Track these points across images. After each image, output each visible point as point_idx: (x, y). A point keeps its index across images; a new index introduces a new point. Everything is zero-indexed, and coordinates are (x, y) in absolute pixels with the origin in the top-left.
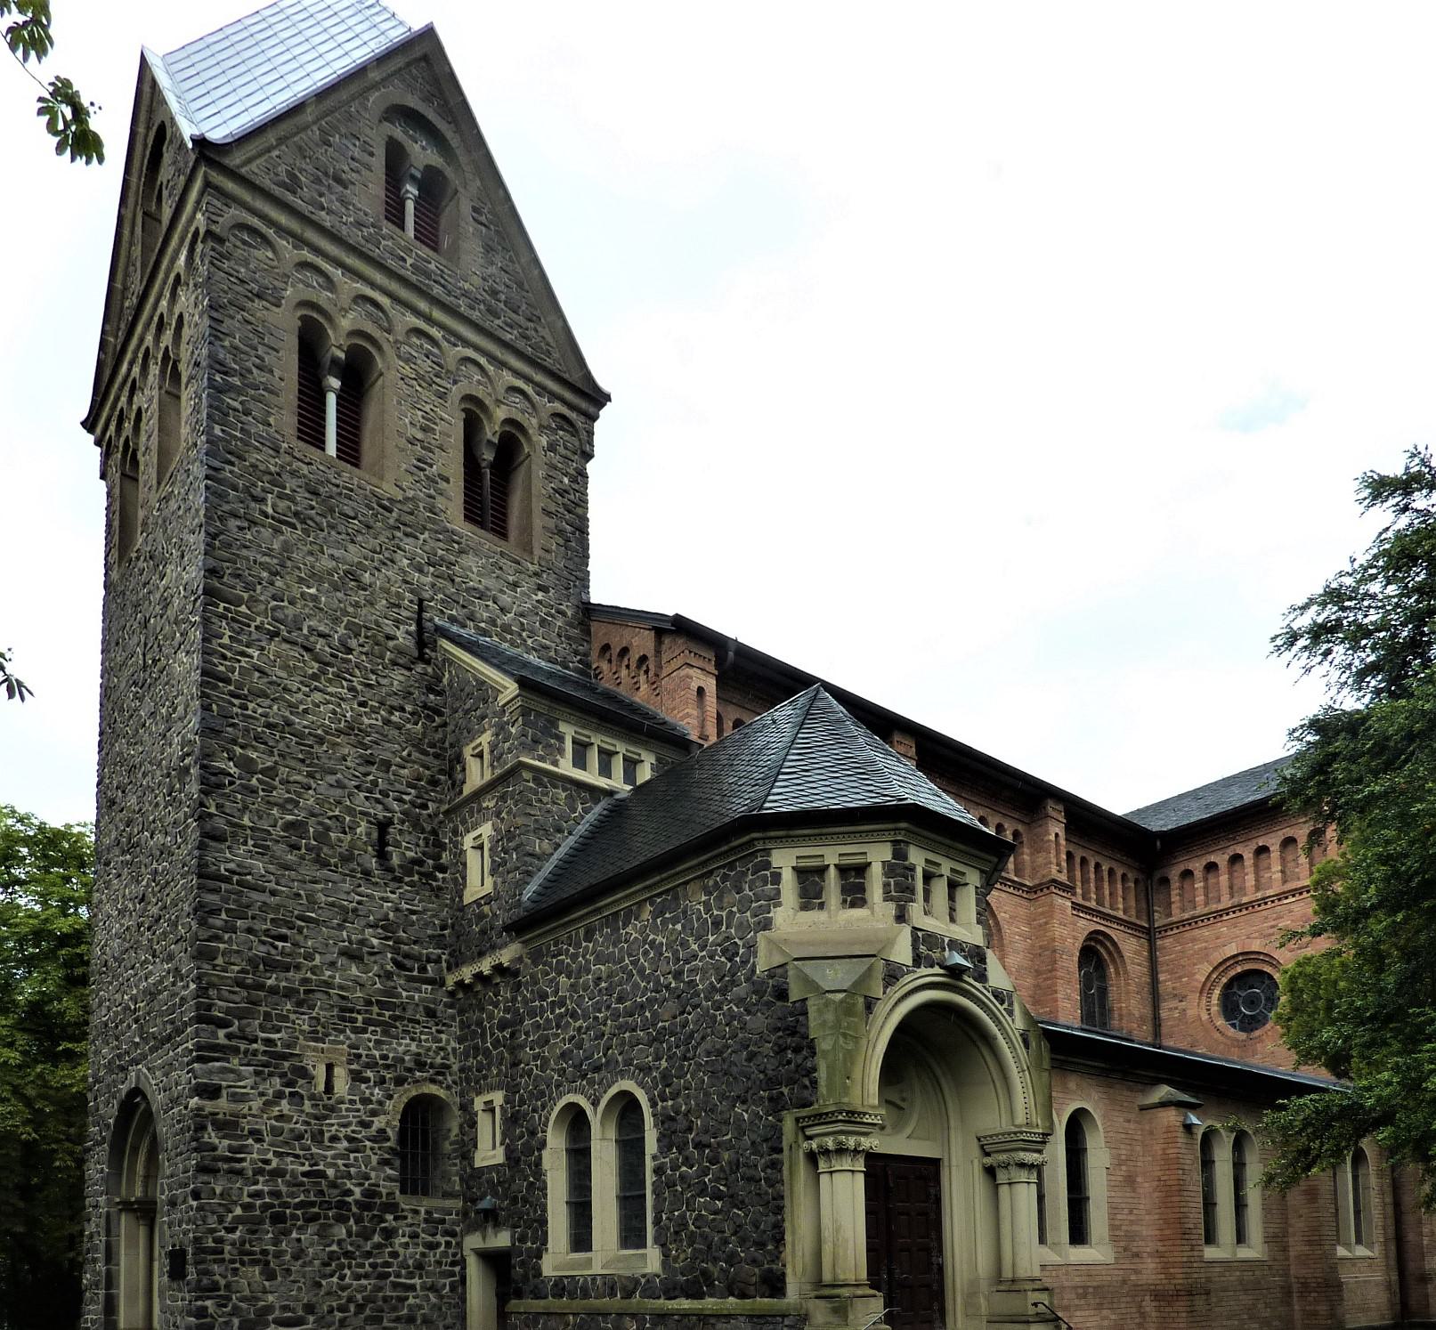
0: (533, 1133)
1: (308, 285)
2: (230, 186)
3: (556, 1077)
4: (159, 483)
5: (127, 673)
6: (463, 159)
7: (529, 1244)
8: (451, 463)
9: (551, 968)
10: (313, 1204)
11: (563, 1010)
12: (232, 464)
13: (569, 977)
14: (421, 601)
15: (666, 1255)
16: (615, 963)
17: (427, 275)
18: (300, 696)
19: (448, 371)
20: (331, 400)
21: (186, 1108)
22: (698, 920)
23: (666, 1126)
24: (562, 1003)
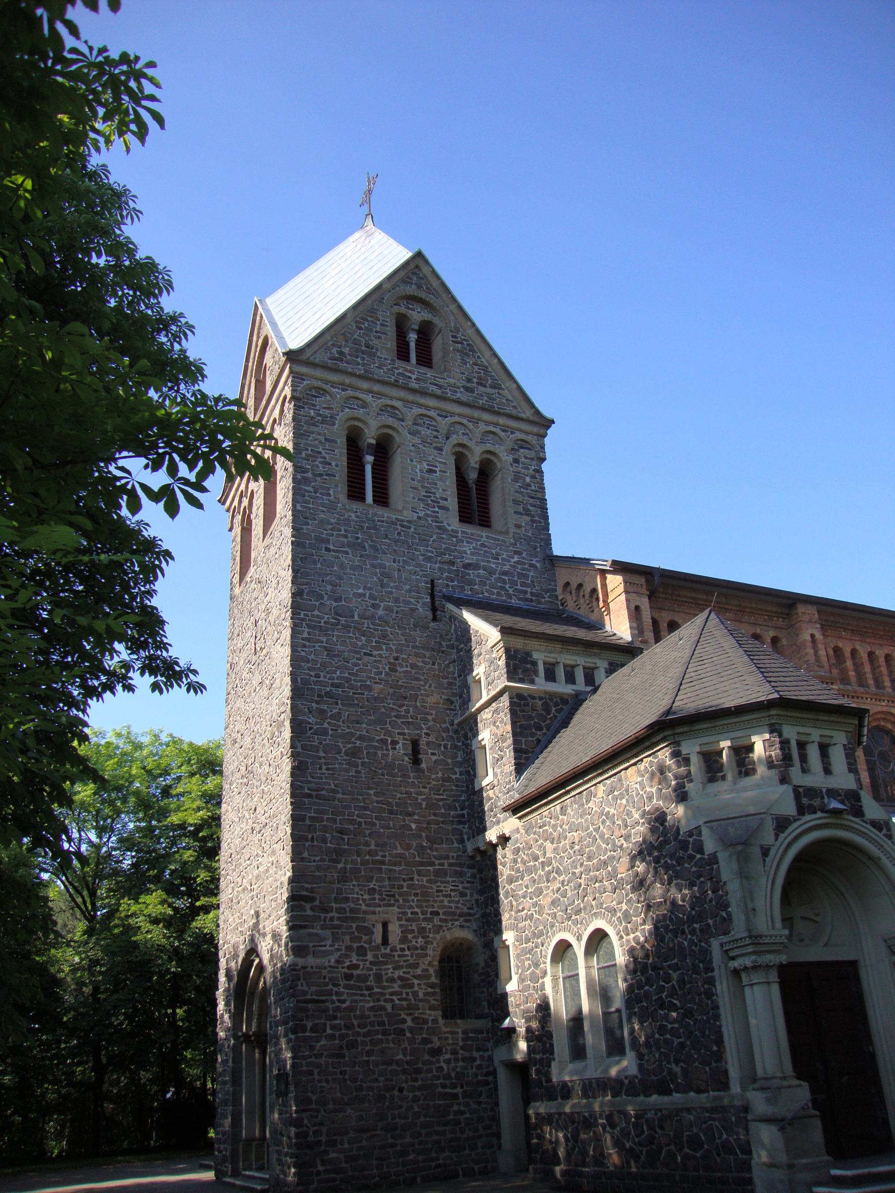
4: (264, 537)
5: (244, 655)
8: (447, 489)
10: (377, 1032)
13: (552, 843)
14: (432, 582)
15: (640, 1057)
20: (368, 469)
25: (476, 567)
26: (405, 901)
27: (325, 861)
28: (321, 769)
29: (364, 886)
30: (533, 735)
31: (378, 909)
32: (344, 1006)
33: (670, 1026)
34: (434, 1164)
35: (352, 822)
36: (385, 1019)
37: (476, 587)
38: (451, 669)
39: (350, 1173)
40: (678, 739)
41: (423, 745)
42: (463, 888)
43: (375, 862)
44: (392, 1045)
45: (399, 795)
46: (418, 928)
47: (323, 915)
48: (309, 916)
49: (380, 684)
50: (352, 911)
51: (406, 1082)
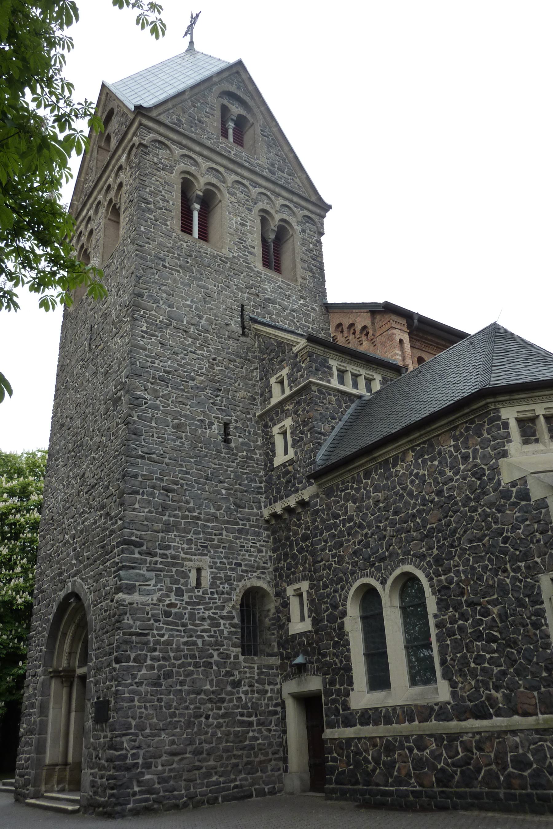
0: (335, 607)
1: (186, 164)
2: (151, 124)
3: (350, 567)
6: (256, 110)
7: (338, 686)
9: (341, 498)
10: (189, 664)
11: (352, 524)
12: (149, 244)
13: (355, 502)
14: (243, 306)
15: (453, 685)
16: (389, 490)
17: (241, 158)
18: (182, 355)
19: (252, 199)
20: (196, 215)
21: (112, 601)
22: (450, 457)
23: (442, 593)
24: (351, 519)
25: (273, 302)
26: (216, 552)
27: (152, 513)
28: (152, 436)
29: (183, 537)
30: (329, 422)
31: (193, 557)
32: (163, 639)
33: (488, 656)
34: (232, 785)
35: (176, 483)
36: (197, 653)
37: (274, 316)
38: (255, 374)
39: (162, 794)
40: (498, 406)
41: (232, 429)
42: (260, 545)
43: (193, 518)
44: (201, 676)
45: (213, 466)
46: (225, 576)
47: (149, 559)
48: (138, 559)
49: (202, 376)
50: (174, 557)
51: (212, 710)
